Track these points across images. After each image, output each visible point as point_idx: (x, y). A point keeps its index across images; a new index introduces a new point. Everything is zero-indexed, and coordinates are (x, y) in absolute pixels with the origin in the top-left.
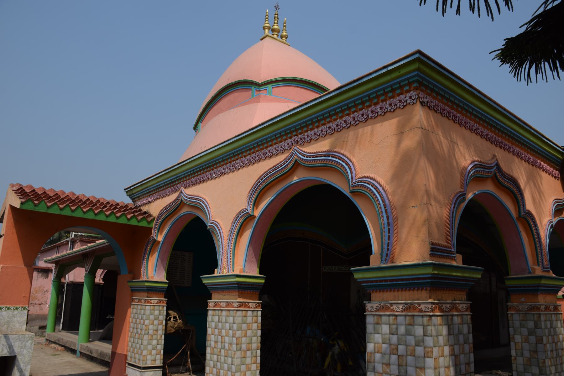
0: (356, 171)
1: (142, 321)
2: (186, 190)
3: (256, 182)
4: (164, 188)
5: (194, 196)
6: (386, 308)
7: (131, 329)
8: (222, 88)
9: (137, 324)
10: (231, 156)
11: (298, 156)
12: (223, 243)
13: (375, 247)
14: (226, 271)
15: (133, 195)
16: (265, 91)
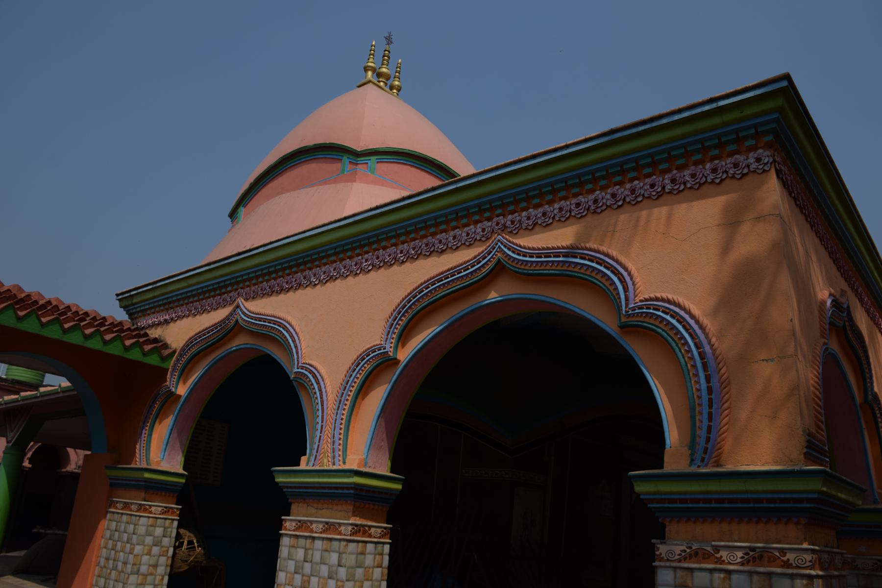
0: (636, 288)
1: (128, 546)
2: (248, 303)
3: (408, 296)
4: (201, 297)
5: (265, 315)
6: (704, 554)
7: (102, 561)
8: (288, 154)
9: (116, 552)
10: (285, 267)
11: (503, 254)
12: (325, 406)
13: (672, 435)
14: (329, 461)
15: (133, 307)
16: (365, 165)
